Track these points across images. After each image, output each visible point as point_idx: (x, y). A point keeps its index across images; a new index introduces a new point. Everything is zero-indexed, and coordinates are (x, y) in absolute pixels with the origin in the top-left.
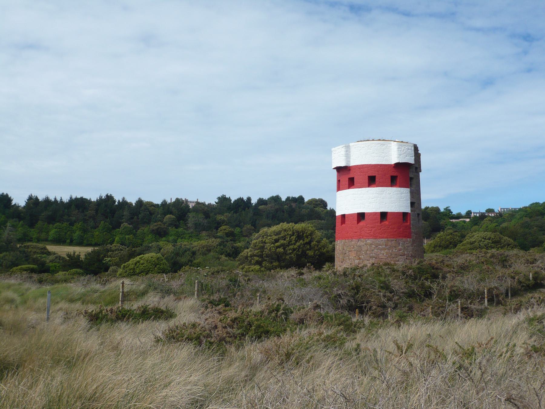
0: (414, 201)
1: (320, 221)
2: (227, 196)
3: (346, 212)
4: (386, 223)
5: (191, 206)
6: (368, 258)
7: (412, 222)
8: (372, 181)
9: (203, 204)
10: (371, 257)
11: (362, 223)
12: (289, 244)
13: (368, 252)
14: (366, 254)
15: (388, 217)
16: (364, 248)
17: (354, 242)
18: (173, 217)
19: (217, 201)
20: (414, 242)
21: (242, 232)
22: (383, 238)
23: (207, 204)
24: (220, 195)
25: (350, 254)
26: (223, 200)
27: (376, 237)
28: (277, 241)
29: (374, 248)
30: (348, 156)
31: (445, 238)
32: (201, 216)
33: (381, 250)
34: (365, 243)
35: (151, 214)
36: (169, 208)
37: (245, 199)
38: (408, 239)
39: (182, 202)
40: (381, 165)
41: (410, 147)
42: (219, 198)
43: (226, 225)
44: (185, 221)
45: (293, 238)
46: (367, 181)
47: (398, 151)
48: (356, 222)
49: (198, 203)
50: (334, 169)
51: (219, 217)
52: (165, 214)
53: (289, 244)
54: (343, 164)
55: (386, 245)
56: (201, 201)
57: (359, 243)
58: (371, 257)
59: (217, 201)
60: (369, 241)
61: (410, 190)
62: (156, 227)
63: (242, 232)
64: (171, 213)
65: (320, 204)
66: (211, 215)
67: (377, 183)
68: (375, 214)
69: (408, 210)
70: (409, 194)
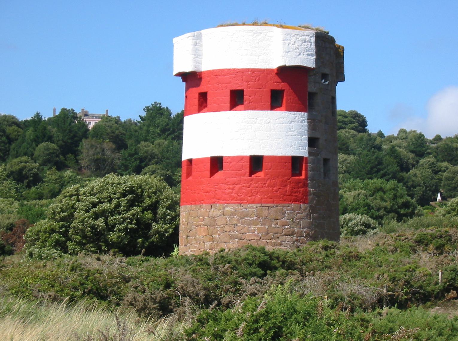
0: (317, 135)
2: (163, 106)
3: (194, 156)
4: (260, 175)
5: (91, 124)
6: (226, 239)
7: (310, 173)
8: (237, 100)
9: (117, 121)
10: (231, 237)
11: (219, 175)
12: (115, 211)
13: (227, 228)
14: (224, 231)
15: (265, 163)
16: (220, 221)
17: (204, 209)
19: (144, 114)
20: (313, 210)
22: (253, 202)
23: (123, 120)
24: (149, 103)
25: (207, 229)
27: (240, 201)
29: (238, 220)
30: (197, 55)
32: (108, 145)
33: (250, 224)
35: (10, 141)
36: (45, 129)
38: (302, 206)
39: (75, 116)
40: (253, 71)
41: (307, 38)
42: (148, 109)
43: (157, 163)
44: (76, 153)
45: (124, 201)
47: (284, 44)
48: (208, 173)
49: (106, 119)
50: (179, 75)
51: (145, 147)
52: (37, 141)
53: (113, 212)
54: (188, 68)
55: (258, 216)
56: (113, 114)
57: (211, 213)
58: (231, 237)
59: (144, 114)
60: (229, 209)
61: (309, 116)
62: (17, 167)
64: (50, 139)
65: (351, 122)
66: (129, 142)
67: (245, 103)
68: (241, 158)
69: (302, 151)
70: (306, 123)
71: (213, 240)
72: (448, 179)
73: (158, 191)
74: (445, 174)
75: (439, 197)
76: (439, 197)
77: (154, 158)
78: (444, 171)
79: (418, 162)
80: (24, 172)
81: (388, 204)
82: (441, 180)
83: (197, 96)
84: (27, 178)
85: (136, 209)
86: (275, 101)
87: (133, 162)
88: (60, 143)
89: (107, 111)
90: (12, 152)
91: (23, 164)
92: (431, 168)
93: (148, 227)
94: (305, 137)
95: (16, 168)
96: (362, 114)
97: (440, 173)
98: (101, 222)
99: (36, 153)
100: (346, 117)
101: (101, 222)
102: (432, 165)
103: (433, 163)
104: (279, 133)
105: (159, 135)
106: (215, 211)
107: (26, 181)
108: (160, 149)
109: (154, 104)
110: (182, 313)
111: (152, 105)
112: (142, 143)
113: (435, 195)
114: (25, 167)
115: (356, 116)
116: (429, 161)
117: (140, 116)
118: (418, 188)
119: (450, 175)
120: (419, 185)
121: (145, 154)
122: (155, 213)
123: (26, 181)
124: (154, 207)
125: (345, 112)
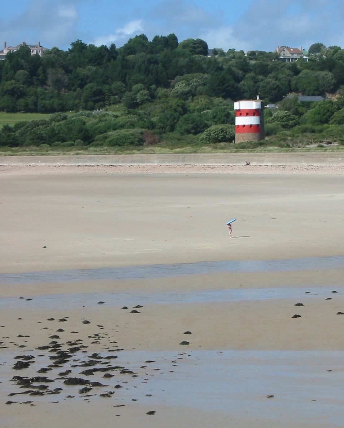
1: (202, 74)
4: (252, 128)
8: (247, 114)
18: (25, 72)
21: (111, 89)
26: (79, 47)
28: (215, 133)
31: (324, 107)
34: (245, 134)
37: (109, 46)
42: (73, 44)
46: (246, 114)
53: (219, 134)
60: (246, 134)
63: (111, 89)
64: (22, 67)
65: (199, 47)
71: (243, 139)
72: (263, 87)
73: (226, 129)
74: (261, 83)
77: (88, 78)
78: (261, 81)
79: (244, 76)
80: (15, 90)
82: (259, 87)
83: (239, 113)
85: (223, 133)
86: (254, 115)
87: (77, 81)
89: (39, 43)
91: (14, 85)
92: (252, 80)
93: (226, 136)
94: (259, 121)
95: (10, 88)
96: (205, 41)
97: (258, 83)
98: (216, 136)
100: (195, 44)
101: (216, 136)
102: (253, 78)
103: (254, 77)
104: (253, 120)
105: (88, 63)
106: (244, 134)
107: (16, 96)
109: (77, 40)
111: (76, 41)
113: (255, 96)
115: (201, 43)
116: (251, 76)
117: (69, 49)
118: (246, 93)
119: (264, 84)
120: (247, 92)
121: (83, 76)
122: (226, 134)
123: (16, 96)
124: (226, 132)
125: (194, 40)
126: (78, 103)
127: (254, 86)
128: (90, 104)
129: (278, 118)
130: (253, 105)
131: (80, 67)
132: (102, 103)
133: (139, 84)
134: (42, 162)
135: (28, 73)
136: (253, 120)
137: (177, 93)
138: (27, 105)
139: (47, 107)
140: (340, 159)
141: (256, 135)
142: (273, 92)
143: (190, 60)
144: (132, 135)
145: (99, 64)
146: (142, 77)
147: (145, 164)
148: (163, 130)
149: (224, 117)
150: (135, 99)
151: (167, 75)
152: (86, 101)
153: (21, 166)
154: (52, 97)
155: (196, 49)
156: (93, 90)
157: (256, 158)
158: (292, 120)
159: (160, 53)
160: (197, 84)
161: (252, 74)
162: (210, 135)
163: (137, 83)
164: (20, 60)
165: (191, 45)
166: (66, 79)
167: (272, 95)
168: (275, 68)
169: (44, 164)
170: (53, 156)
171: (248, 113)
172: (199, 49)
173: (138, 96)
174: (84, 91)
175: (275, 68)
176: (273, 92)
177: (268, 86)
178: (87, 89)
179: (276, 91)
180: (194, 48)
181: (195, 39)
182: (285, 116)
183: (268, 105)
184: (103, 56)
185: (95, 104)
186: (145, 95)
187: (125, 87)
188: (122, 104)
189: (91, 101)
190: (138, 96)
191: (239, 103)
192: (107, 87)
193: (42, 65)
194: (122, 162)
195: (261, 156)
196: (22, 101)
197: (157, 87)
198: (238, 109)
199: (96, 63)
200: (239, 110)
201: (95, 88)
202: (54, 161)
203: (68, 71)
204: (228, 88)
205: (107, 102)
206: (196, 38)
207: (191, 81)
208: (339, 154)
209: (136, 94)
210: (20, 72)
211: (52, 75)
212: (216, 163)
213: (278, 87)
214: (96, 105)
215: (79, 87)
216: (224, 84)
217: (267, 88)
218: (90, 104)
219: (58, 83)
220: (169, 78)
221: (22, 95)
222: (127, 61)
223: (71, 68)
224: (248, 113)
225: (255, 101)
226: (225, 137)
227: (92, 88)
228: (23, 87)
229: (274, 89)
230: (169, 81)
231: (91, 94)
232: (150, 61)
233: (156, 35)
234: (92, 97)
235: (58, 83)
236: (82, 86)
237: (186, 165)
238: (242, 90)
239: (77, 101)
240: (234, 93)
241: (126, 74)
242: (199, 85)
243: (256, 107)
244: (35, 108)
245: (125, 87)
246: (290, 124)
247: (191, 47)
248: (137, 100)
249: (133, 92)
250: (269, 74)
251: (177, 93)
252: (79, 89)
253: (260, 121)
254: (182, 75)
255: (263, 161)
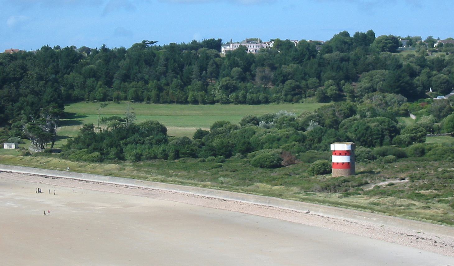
4: (344, 165)
8: (340, 154)
11: (338, 165)
12: (321, 167)
27: (341, 168)
64: (237, 65)
65: (390, 43)
72: (435, 81)
75: (431, 90)
76: (431, 90)
79: (421, 70)
81: (386, 127)
82: (432, 80)
84: (230, 88)
86: (346, 155)
88: (242, 66)
90: (221, 74)
91: (228, 81)
99: (232, 74)
103: (428, 72)
104: (345, 159)
105: (292, 61)
106: (338, 170)
108: (293, 69)
110: (262, 82)
112: (283, 66)
114: (229, 83)
126: (280, 96)
127: (427, 81)
128: (289, 97)
129: (409, 130)
130: (345, 147)
131: (285, 64)
132: (299, 96)
133: (330, 81)
134: (180, 190)
135: (241, 70)
136: (345, 159)
137: (361, 88)
138: (237, 97)
139: (253, 100)
140: (364, 218)
141: (347, 170)
142: (443, 86)
143: (376, 58)
144: (273, 155)
145: (301, 62)
146: (334, 74)
147: (245, 202)
148: (312, 142)
149: (364, 130)
150: (326, 93)
151: (357, 70)
152: (286, 95)
153: (166, 192)
154: (259, 91)
155: (387, 44)
156: (292, 85)
157: (313, 208)
158: (420, 132)
159: (353, 51)
160: (379, 80)
161: (427, 70)
162: (314, 168)
163: (329, 79)
164: (236, 58)
165: (383, 41)
166: (272, 75)
167: (442, 88)
168: (450, 62)
169: (181, 192)
170: (187, 187)
171: (341, 153)
172: (391, 44)
173: (328, 90)
174: (285, 86)
175: (450, 62)
176: (443, 86)
177: (439, 81)
178: (287, 85)
179: (446, 85)
180: (386, 43)
181: (388, 36)
182: (414, 129)
183: (438, 97)
184: (304, 55)
185: (293, 97)
186: (334, 90)
187: (318, 83)
188: (315, 97)
189: (290, 94)
190: (328, 90)
191: (334, 145)
192: (303, 83)
193: (255, 63)
194: (231, 198)
195: (317, 207)
196: (234, 95)
197: (345, 82)
198: (333, 150)
199: (298, 61)
200: (334, 151)
201: (293, 83)
202: (188, 191)
203: (273, 68)
204: (402, 84)
205: (303, 95)
206: (389, 34)
207: (374, 77)
208: (364, 214)
209: (327, 89)
210: (235, 69)
211: (258, 72)
212: (289, 208)
213: (447, 81)
214: (294, 98)
215: (281, 83)
216: (399, 81)
217: (438, 83)
218: (289, 97)
219: (265, 78)
220: (358, 73)
221: (235, 89)
222: (324, 59)
223: (277, 65)
224: (341, 153)
225: (347, 144)
226: (325, 169)
227: (291, 84)
228: (235, 83)
229: (445, 83)
230: (359, 75)
231: (290, 89)
232: (342, 60)
233: (356, 31)
234: (291, 92)
235: (265, 78)
236: (283, 82)
237: (270, 206)
238: (415, 85)
239: (278, 95)
240: (408, 88)
241: (321, 71)
242: (380, 81)
243: (347, 148)
244: (244, 100)
245: (318, 83)
246: (418, 136)
247: (383, 43)
248: (327, 94)
249: (324, 87)
250: (444, 68)
251: (361, 88)
252: (281, 84)
253: (351, 160)
254: (368, 71)
255: (318, 211)
